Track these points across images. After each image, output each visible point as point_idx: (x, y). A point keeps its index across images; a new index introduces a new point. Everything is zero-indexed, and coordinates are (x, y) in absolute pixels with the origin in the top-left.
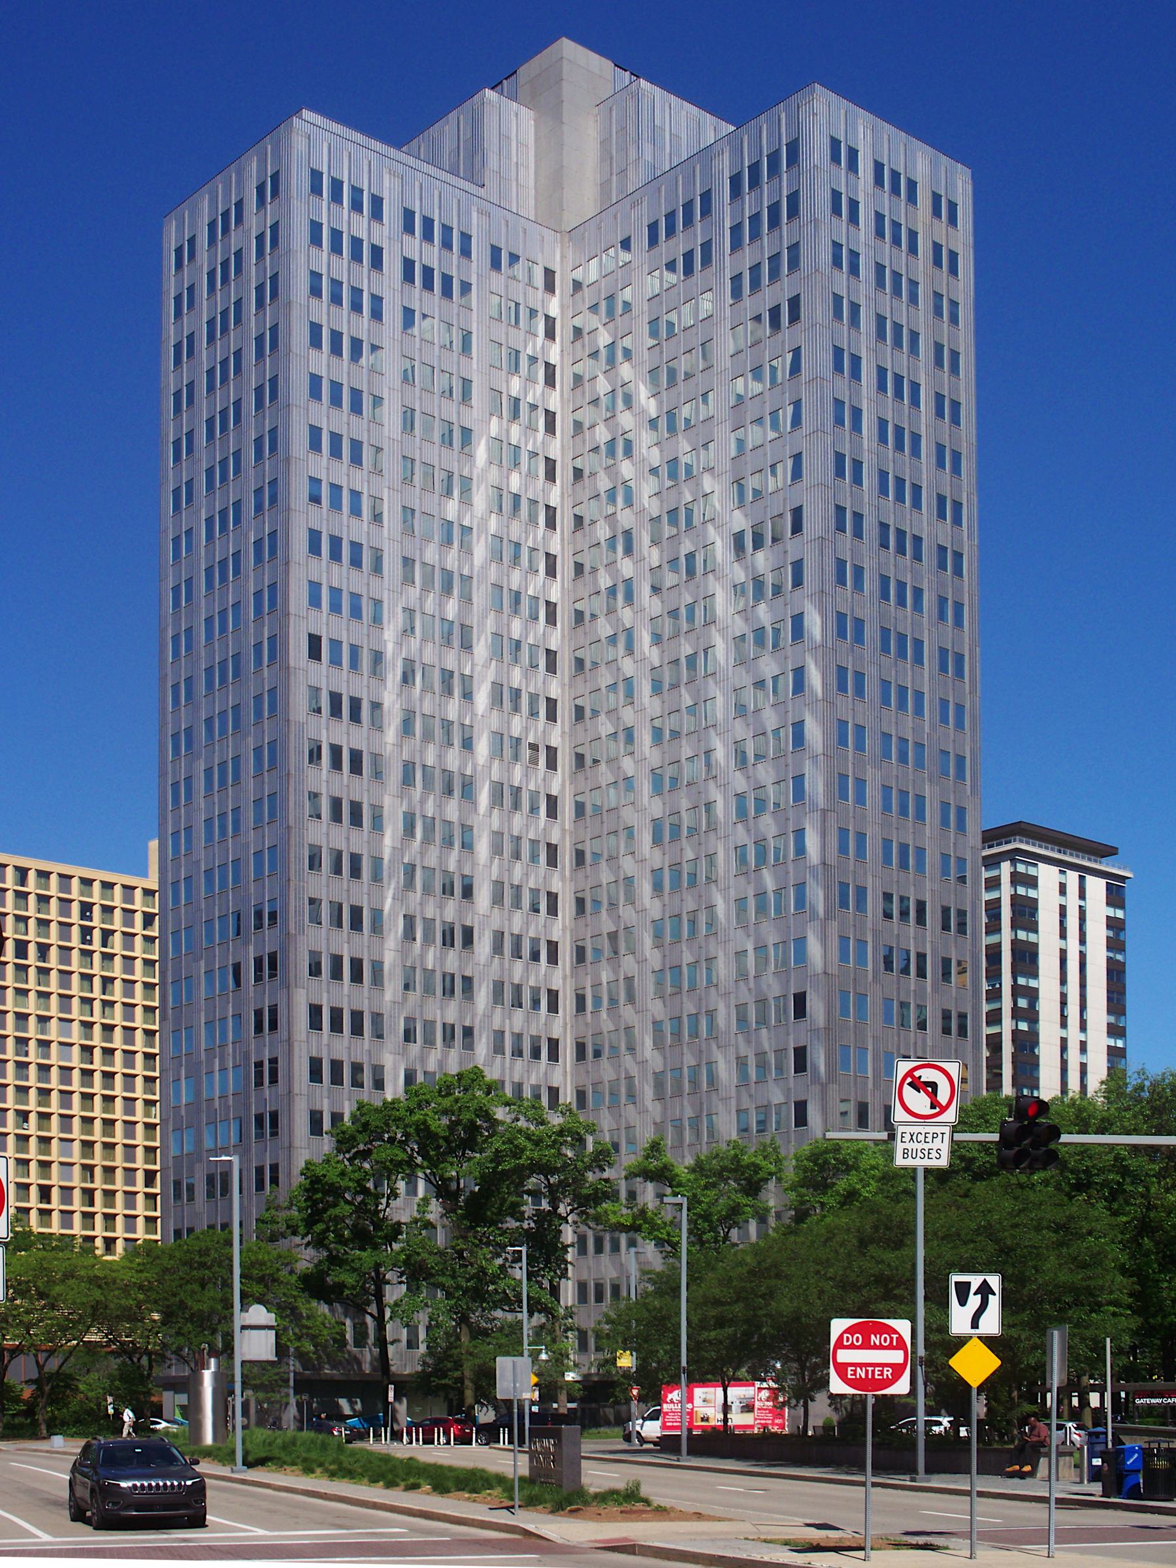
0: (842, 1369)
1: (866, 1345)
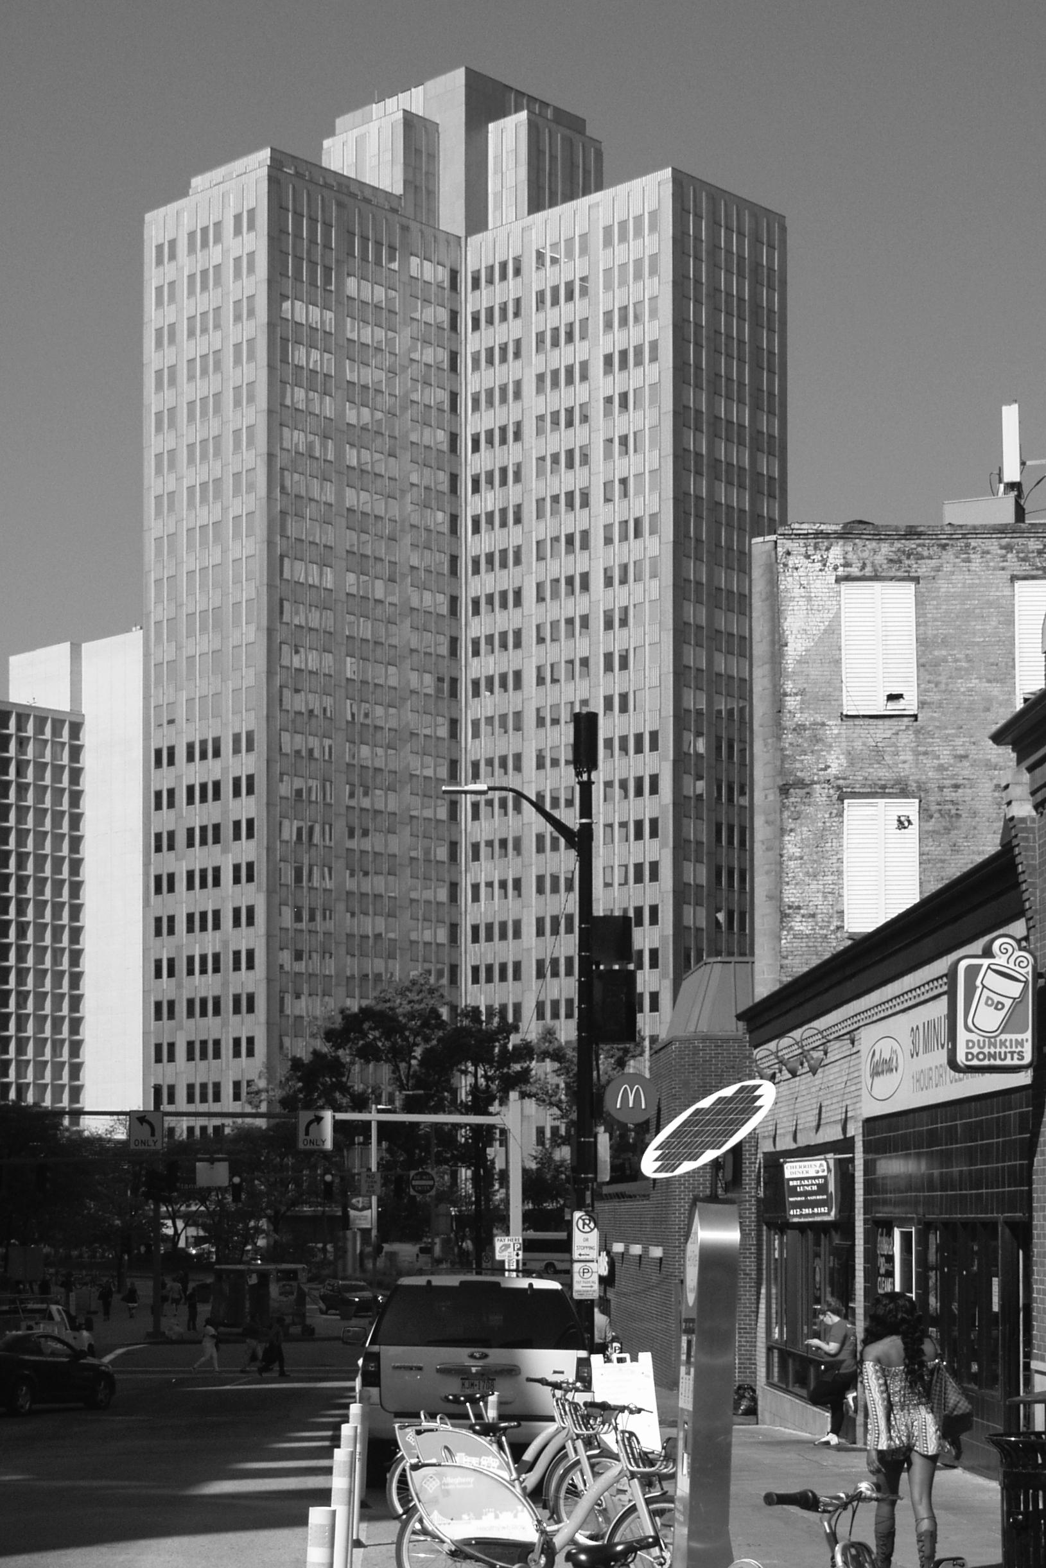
0: (414, 1187)
1: (421, 1179)
